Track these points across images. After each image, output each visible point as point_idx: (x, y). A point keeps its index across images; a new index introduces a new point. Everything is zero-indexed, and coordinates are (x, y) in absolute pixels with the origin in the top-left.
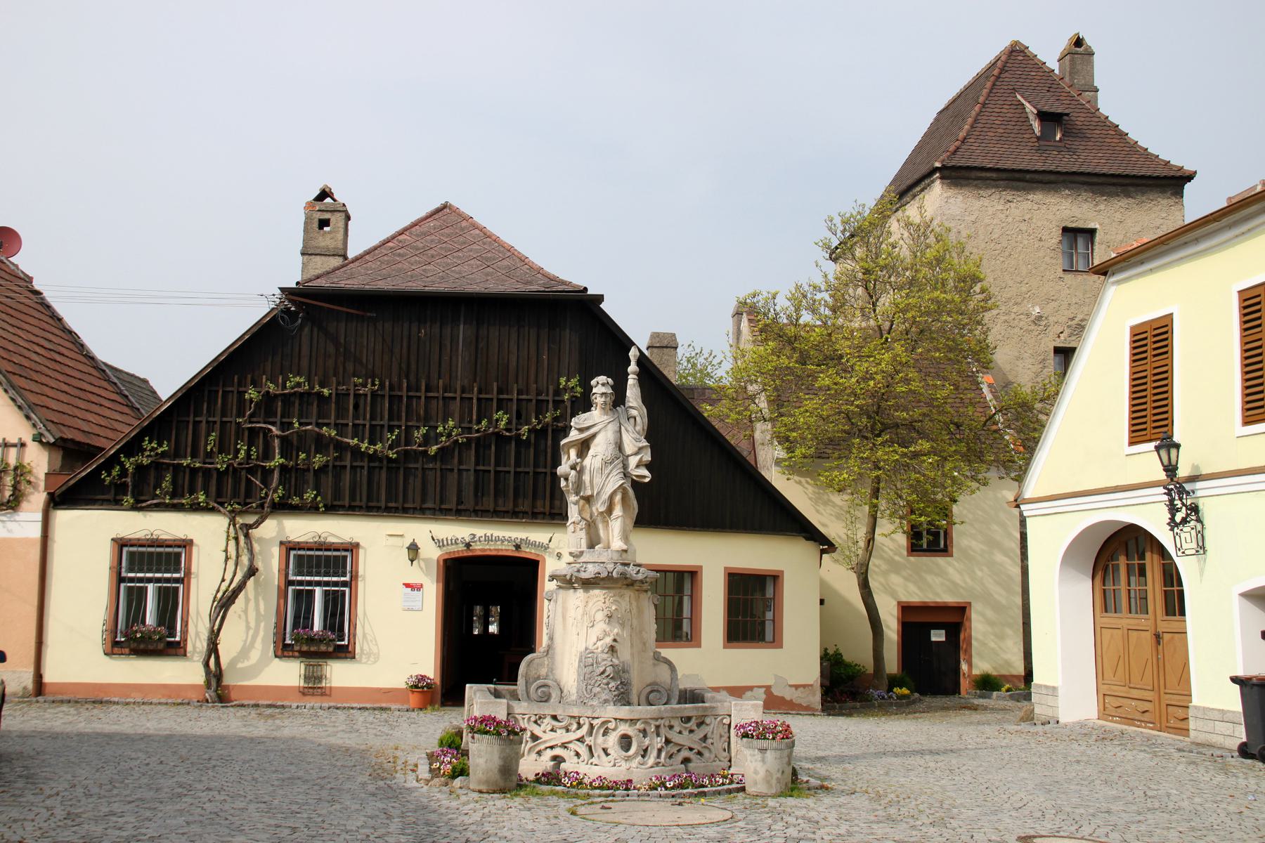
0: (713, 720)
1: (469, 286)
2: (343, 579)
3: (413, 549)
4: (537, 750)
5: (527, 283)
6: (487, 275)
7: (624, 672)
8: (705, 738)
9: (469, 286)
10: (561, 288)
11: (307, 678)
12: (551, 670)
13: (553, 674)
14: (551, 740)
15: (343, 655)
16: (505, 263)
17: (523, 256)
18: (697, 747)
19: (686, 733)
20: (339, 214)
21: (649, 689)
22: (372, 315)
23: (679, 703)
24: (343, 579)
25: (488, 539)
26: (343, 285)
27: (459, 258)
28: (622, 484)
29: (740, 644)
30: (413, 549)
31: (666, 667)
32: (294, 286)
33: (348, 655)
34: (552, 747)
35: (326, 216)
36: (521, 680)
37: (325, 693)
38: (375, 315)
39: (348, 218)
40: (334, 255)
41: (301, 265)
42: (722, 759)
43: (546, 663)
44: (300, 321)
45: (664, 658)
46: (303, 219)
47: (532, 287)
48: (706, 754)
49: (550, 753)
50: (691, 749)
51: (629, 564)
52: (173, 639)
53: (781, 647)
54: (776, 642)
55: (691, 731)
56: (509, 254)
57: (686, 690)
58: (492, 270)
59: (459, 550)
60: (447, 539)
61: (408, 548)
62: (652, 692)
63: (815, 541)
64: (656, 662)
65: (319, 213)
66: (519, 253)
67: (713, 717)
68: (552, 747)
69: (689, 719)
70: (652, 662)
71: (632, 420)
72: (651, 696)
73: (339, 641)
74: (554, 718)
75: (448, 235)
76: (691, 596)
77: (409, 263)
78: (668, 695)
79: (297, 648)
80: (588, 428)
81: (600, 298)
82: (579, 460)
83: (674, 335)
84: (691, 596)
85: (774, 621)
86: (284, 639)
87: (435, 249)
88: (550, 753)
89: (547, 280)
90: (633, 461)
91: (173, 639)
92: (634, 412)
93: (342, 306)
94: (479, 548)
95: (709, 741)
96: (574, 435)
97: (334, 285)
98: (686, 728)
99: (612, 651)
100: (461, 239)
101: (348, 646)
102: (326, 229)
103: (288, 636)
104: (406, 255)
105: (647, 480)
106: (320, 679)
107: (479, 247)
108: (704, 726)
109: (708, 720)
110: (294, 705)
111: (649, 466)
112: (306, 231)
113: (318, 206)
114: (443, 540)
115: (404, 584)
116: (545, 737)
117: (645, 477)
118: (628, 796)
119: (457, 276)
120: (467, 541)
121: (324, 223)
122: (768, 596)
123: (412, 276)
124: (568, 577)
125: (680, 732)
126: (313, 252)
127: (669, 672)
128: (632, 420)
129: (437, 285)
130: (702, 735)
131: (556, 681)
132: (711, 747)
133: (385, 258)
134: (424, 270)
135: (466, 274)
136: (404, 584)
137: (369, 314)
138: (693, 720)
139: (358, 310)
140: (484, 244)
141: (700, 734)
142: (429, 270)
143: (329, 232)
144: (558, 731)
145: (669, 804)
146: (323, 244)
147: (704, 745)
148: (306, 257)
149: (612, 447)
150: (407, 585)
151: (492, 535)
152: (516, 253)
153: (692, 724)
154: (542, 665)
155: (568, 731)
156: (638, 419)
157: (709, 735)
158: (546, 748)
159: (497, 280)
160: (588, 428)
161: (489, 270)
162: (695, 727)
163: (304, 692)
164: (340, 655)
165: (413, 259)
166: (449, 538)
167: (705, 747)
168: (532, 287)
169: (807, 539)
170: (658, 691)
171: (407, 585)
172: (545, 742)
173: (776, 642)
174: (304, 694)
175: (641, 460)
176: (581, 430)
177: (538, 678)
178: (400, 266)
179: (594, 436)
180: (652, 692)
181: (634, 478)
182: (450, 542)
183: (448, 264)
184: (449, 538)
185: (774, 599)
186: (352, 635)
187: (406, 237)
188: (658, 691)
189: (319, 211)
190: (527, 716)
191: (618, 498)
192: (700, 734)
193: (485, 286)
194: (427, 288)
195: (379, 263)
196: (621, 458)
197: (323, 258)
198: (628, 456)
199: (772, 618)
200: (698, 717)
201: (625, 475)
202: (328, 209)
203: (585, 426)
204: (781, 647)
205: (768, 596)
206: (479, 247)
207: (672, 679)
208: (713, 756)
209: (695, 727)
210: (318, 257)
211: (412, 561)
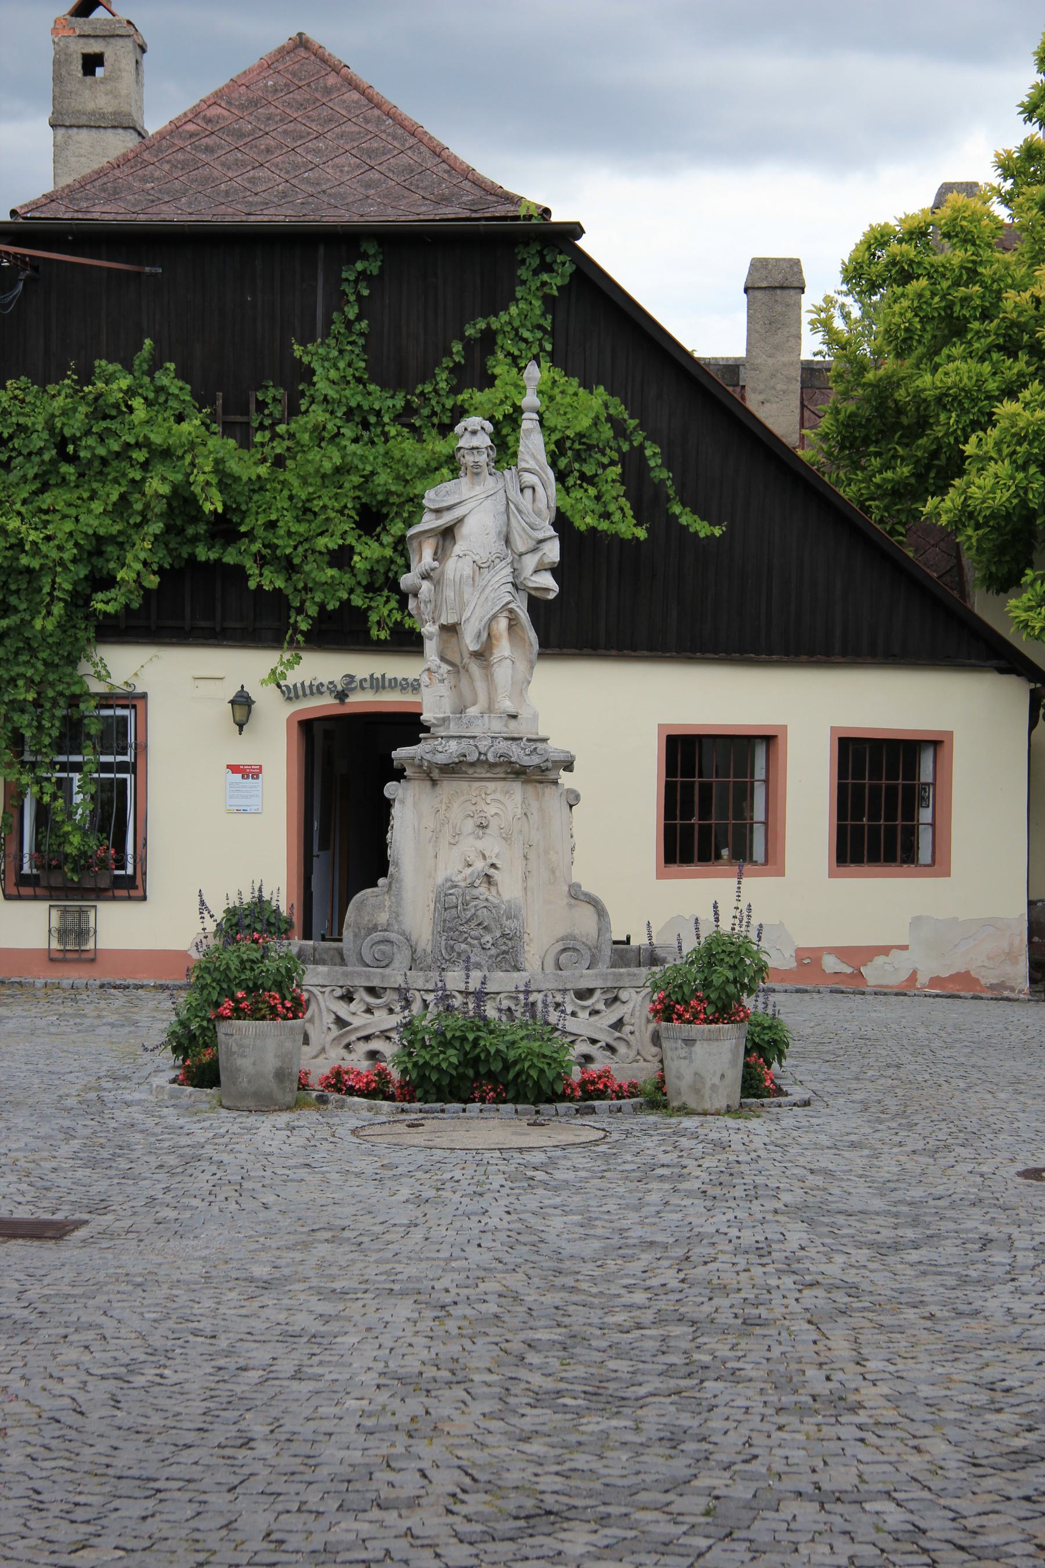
0: (634, 995)
1: (332, 212)
2: (120, 758)
3: (242, 703)
4: (345, 1042)
5: (444, 200)
6: (368, 186)
7: (508, 918)
8: (619, 1025)
9: (332, 212)
10: (500, 210)
11: (63, 934)
12: (397, 915)
13: (399, 922)
14: (364, 1026)
15: (123, 893)
16: (404, 160)
17: (439, 144)
18: (605, 1038)
19: (584, 1015)
20: (120, 42)
21: (560, 946)
22: (154, 270)
23: (613, 966)
24: (120, 758)
25: (378, 684)
26: (96, 216)
27: (317, 152)
28: (508, 603)
29: (866, 868)
30: (242, 703)
31: (588, 911)
32: (8, 218)
33: (133, 893)
34: (367, 1038)
35: (94, 47)
36: (347, 934)
37: (92, 959)
38: (160, 270)
39: (143, 49)
40: (114, 127)
41: (52, 149)
42: (650, 1058)
43: (387, 904)
44: (21, 285)
45: (586, 895)
46: (52, 54)
47: (447, 210)
48: (622, 1049)
49: (363, 1047)
50: (594, 1041)
51: (521, 739)
52: (122, 872)
53: (947, 874)
54: (939, 865)
55: (595, 1012)
56: (412, 141)
57: (640, 948)
58: (377, 176)
59: (324, 704)
60: (303, 684)
61: (232, 702)
62: (564, 950)
63: (1019, 674)
64: (573, 901)
65: (82, 41)
66: (431, 138)
67: (632, 990)
68: (367, 1038)
69: (590, 992)
70: (566, 900)
71: (528, 492)
72: (563, 958)
73: (117, 868)
74: (372, 991)
75: (301, 106)
76: (766, 781)
77: (223, 164)
78: (593, 956)
79: (44, 883)
80: (449, 508)
81: (575, 230)
82: (436, 564)
83: (796, 263)
84: (766, 781)
85: (933, 825)
86: (21, 867)
87: (273, 134)
88: (363, 1047)
89: (479, 193)
90: (530, 562)
91: (122, 872)
92: (529, 478)
93: (99, 258)
94: (361, 700)
95: (627, 1029)
96: (428, 522)
97: (80, 216)
98: (584, 1008)
99: (489, 883)
100: (325, 112)
101: (133, 877)
102: (99, 71)
103: (26, 860)
104: (220, 147)
105: (552, 596)
106: (82, 934)
107: (356, 129)
108: (618, 1003)
109: (624, 995)
110: (39, 983)
111: (556, 572)
112: (58, 79)
113: (82, 24)
114: (295, 686)
115: (229, 767)
116: (356, 1022)
117: (547, 590)
118: (464, 1110)
119: (310, 189)
120: (339, 688)
121: (91, 63)
122: (923, 779)
123: (227, 193)
124: (417, 762)
125: (574, 1014)
126: (74, 122)
127: (595, 917)
128: (528, 492)
129: (272, 211)
130: (613, 1019)
131: (403, 934)
132: (631, 1038)
133: (180, 156)
134: (252, 180)
135: (329, 185)
136: (229, 767)
137: (147, 269)
138: (597, 994)
139: (127, 262)
140: (367, 121)
141: (611, 1016)
142: (259, 178)
143: (104, 80)
144: (377, 1013)
145: (524, 1123)
146: (91, 106)
147: (617, 1034)
148: (61, 131)
149: (493, 537)
150: (234, 769)
151: (383, 676)
152: (425, 140)
153: (596, 1001)
154: (381, 907)
155: (391, 1011)
156: (540, 489)
157: (626, 1020)
158: (359, 1039)
159: (386, 196)
160: (449, 508)
161: (374, 175)
162: (601, 1006)
163: (53, 959)
164: (119, 893)
165: (230, 157)
166: (307, 684)
167: (619, 1038)
168: (447, 210)
169: (1002, 671)
170: (575, 949)
171: (234, 769)
172: (356, 1029)
173: (939, 865)
174: (52, 960)
175: (540, 562)
176: (438, 511)
177: (375, 928)
178: (207, 171)
179: (460, 521)
180: (564, 950)
181: (533, 593)
182: (308, 691)
183: (296, 167)
184: (307, 684)
185: (934, 784)
186: (141, 860)
187: (220, 110)
188: (575, 949)
189: (80, 36)
190: (328, 989)
191: (503, 623)
192: (611, 1016)
193: (361, 211)
194: (252, 218)
195: (167, 167)
196: (509, 559)
197: (94, 133)
198: (521, 555)
199: (930, 821)
200: (606, 990)
201: (514, 585)
202: (98, 33)
203: (445, 504)
204: (947, 874)
205: (923, 779)
206: (356, 129)
207: (599, 930)
208: (632, 1054)
209: (601, 1006)
210: (84, 132)
211: (241, 726)
